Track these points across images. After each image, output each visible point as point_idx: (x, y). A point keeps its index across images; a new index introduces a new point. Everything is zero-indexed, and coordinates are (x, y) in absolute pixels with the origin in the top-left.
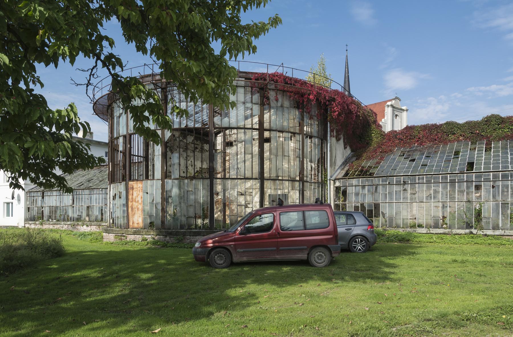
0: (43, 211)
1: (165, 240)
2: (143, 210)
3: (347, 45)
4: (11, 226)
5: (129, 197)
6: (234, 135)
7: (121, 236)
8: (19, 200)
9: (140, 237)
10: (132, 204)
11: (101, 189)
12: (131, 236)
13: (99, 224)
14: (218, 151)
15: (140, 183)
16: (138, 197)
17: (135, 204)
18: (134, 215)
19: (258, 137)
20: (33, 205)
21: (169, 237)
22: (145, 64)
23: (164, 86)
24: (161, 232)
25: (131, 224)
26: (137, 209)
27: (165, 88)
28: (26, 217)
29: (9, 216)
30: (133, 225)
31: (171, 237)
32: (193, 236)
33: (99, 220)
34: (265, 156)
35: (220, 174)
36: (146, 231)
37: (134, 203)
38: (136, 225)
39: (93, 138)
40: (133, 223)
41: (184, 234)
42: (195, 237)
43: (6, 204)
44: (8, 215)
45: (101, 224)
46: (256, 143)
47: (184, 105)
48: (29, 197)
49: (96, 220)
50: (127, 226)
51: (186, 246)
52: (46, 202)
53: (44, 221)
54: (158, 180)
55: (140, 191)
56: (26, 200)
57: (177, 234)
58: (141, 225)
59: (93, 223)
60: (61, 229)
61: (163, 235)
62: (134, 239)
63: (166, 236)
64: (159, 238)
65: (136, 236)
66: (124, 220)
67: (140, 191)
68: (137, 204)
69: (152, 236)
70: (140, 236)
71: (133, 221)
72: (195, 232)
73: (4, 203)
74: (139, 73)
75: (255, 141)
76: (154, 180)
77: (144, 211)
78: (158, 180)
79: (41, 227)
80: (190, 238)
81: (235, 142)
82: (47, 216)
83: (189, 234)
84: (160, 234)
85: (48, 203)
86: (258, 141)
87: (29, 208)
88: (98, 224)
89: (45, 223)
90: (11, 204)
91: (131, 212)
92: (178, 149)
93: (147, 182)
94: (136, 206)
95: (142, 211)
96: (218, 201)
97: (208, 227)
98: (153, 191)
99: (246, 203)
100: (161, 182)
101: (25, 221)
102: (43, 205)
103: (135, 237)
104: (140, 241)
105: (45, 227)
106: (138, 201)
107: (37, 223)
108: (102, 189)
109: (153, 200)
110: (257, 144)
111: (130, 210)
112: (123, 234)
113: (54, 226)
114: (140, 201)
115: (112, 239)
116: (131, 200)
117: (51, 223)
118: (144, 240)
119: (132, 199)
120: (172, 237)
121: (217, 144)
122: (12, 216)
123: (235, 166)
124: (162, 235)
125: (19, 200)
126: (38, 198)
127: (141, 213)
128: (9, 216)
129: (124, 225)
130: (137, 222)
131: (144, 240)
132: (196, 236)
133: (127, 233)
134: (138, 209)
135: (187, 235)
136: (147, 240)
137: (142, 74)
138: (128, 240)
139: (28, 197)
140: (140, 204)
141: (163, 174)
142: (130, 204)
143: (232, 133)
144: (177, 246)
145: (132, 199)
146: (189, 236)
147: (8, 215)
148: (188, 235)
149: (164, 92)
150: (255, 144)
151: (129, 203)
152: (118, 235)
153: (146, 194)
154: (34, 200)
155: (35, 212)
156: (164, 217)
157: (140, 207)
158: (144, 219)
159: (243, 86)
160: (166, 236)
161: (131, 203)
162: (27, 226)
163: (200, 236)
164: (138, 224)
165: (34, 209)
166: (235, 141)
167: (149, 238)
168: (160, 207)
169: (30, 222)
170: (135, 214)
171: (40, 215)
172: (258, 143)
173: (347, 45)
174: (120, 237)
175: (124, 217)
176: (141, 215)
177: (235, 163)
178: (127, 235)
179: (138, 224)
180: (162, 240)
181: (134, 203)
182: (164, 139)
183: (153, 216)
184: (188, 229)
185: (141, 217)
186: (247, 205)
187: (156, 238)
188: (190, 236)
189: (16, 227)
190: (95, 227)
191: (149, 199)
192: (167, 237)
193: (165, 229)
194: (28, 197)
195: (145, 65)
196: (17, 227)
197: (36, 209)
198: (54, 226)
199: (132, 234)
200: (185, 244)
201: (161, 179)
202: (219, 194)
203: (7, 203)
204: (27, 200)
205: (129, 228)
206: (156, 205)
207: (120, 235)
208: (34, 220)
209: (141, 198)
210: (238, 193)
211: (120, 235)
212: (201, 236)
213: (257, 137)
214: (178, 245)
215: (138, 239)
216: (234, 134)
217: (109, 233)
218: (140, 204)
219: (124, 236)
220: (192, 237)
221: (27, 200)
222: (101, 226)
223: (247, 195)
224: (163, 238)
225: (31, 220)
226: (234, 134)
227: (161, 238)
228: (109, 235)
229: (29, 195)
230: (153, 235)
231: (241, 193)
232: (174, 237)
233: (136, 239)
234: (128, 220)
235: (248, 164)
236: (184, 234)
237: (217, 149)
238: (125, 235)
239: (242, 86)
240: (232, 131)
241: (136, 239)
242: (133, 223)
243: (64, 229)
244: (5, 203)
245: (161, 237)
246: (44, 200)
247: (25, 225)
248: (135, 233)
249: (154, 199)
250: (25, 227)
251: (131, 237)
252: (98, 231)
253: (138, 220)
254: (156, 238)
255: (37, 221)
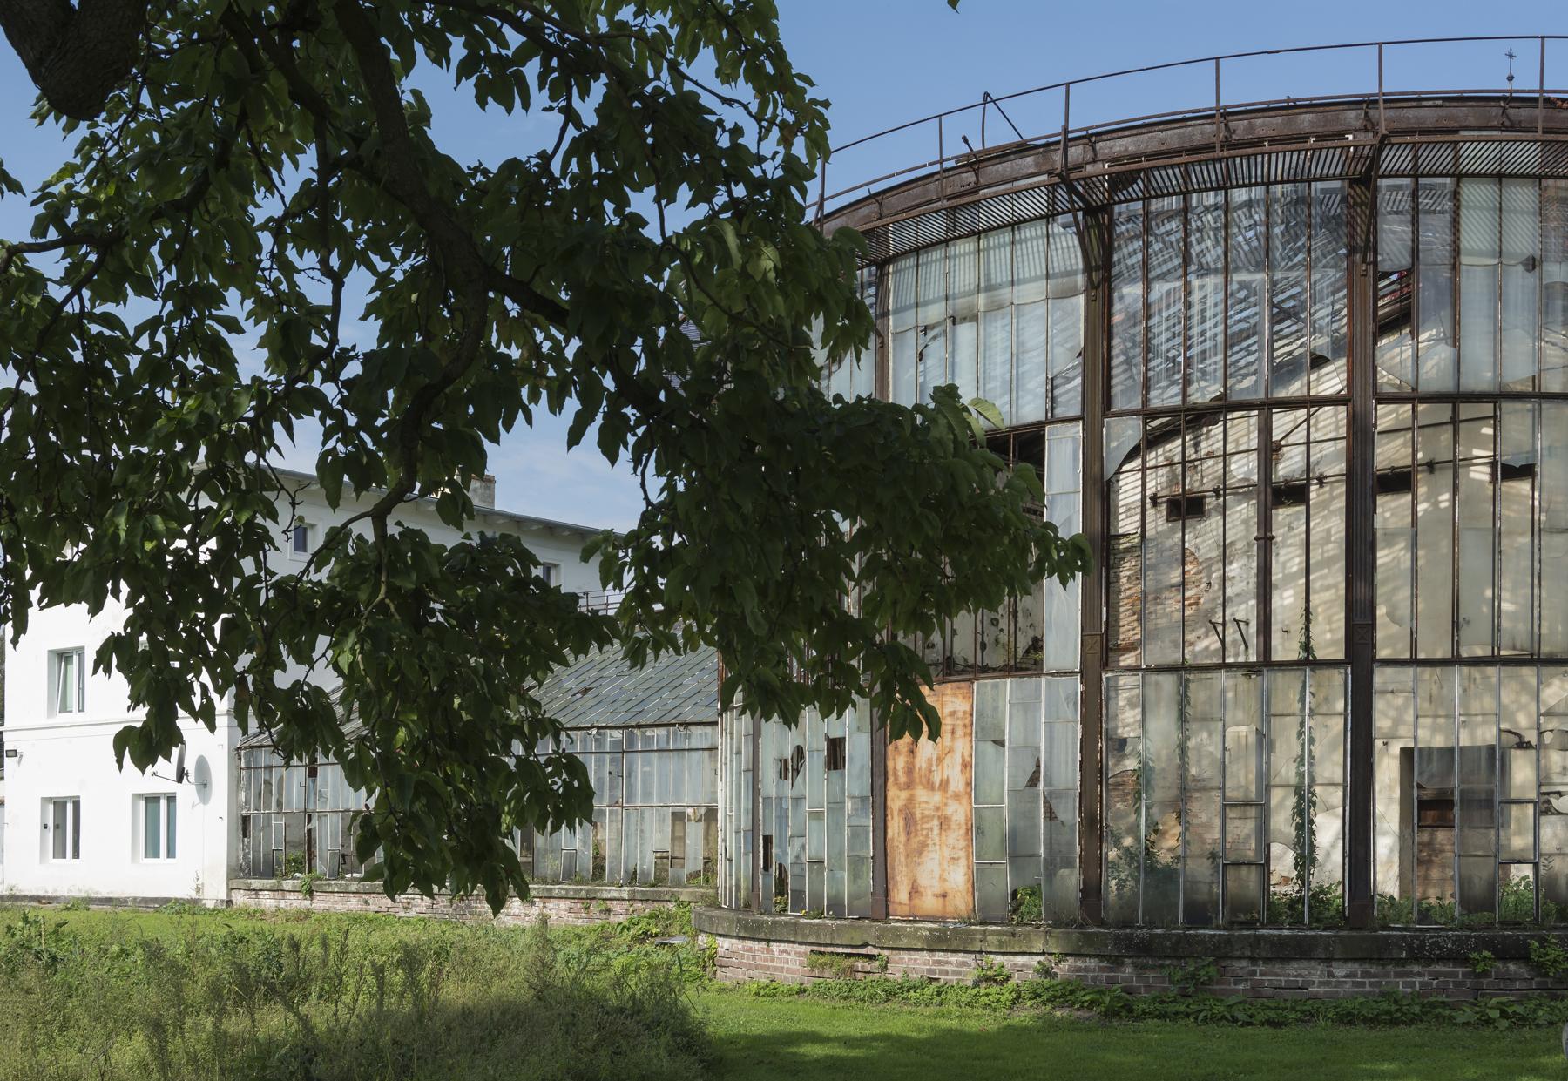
0: (309, 831)
1: (1114, 982)
2: (977, 830)
3: (1511, 56)
4: (177, 900)
5: (890, 765)
6: (1210, 462)
7: (849, 955)
8: (204, 784)
9: (964, 964)
10: (911, 799)
11: (594, 732)
12: (915, 955)
13: (588, 892)
14: (1125, 544)
15: (955, 695)
16: (947, 760)
17: (926, 799)
18: (920, 853)
19: (1344, 465)
20: (268, 806)
21: (1135, 966)
22: (987, 95)
23: (1098, 197)
24: (1088, 939)
25: (900, 894)
26: (936, 822)
27: (1106, 208)
28: (234, 863)
29: (64, 857)
30: (916, 901)
31: (1144, 967)
32: (1267, 960)
33: (584, 873)
34: (1379, 562)
35: (1133, 654)
36: (1000, 934)
37: (921, 794)
38: (929, 904)
39: (493, 502)
40: (914, 891)
41: (1221, 952)
42: (1277, 968)
43: (142, 803)
44: (152, 850)
45: (596, 891)
46: (1333, 498)
47: (1210, 288)
48: (248, 768)
49: (570, 875)
50: (881, 905)
51: (1241, 1016)
52: (329, 792)
53: (319, 879)
54: (1066, 673)
55: (959, 732)
56: (235, 783)
57: (1180, 950)
58: (961, 902)
59: (556, 889)
60: (402, 914)
61: (1101, 957)
62: (929, 971)
63: (1116, 961)
64: (1079, 969)
65: (940, 956)
66: (855, 876)
67: (959, 732)
68: (937, 797)
69: (1041, 958)
70: (969, 958)
71: (915, 881)
72: (1281, 943)
73: (137, 796)
74: (965, 140)
75: (1327, 488)
76: (1040, 674)
77: (980, 831)
78: (1066, 673)
79: (308, 903)
80: (1253, 973)
81: (1218, 496)
82: (334, 854)
83: (1248, 953)
84: (1084, 950)
85: (336, 798)
86: (1344, 489)
87: (245, 820)
88: (583, 894)
89: (326, 888)
90: (163, 803)
91: (903, 838)
92: (1127, 524)
93: (995, 686)
94: (931, 806)
95: (968, 830)
96: (1123, 784)
97: (1340, 913)
98: (1036, 730)
99: (1544, 789)
100: (1080, 688)
101: (229, 879)
102: (311, 808)
103: (939, 962)
104: (970, 983)
105: (321, 903)
106: (945, 785)
107: (288, 884)
108: (599, 728)
109: (1033, 781)
110: (1340, 503)
111: (895, 827)
112: (865, 945)
113: (366, 902)
114: (958, 783)
115: (793, 972)
116: (903, 779)
117: (354, 887)
118: (988, 979)
119: (910, 770)
120: (1153, 968)
121: (1121, 510)
122: (76, 855)
123: (1213, 611)
124: (1097, 956)
125: (205, 785)
126: (290, 777)
127: (962, 843)
128: (64, 857)
129: (856, 903)
130: (938, 890)
131: (988, 979)
132: (1286, 960)
133: (891, 944)
134: (945, 823)
135: (1232, 958)
136: (1008, 978)
137: (977, 147)
138: (895, 974)
139: (244, 772)
140: (957, 796)
141: (1089, 641)
142: (896, 798)
143: (1203, 453)
144: (1188, 1015)
145: (910, 770)
146: (1244, 963)
147: (152, 850)
148: (1239, 958)
149: (1099, 226)
150: (1324, 505)
151: (892, 792)
152: (830, 949)
153: (990, 748)
154: (268, 783)
155: (275, 835)
156: (1093, 863)
157: (959, 812)
158: (978, 878)
159: (1491, 175)
160: (1116, 961)
161: (904, 795)
162: (240, 898)
163: (1304, 964)
164: (944, 896)
165: (270, 825)
166: (1216, 492)
167: (1024, 967)
168: (1071, 814)
169: (256, 883)
170: (924, 845)
171: (299, 853)
172: (1344, 498)
173: (1511, 56)
174: (847, 963)
175: (857, 862)
176: (962, 854)
177: (1214, 599)
178: (886, 952)
179: (944, 896)
180: (1094, 979)
181: (921, 794)
182: (1098, 464)
183: (1036, 855)
184: (1231, 925)
185: (963, 862)
186: (1548, 802)
187: (1064, 968)
188: (1253, 959)
189: (191, 907)
190: (563, 905)
191: (1006, 772)
192: (1122, 964)
193: (1103, 924)
194: (244, 772)
195: (985, 102)
196: (195, 902)
197: (278, 823)
198: (366, 902)
199: (922, 950)
200: (1231, 1001)
201: (1081, 672)
202: (1128, 750)
203: (55, 803)
204: (239, 782)
205: (887, 914)
206: (1054, 803)
207: (840, 950)
208: (272, 875)
209: (965, 766)
210: (1504, 736)
211: (840, 950)
212: (1313, 963)
213: (1341, 467)
214: (1194, 1007)
215: (955, 973)
216: (1210, 456)
217: (768, 941)
218: (957, 796)
219: (872, 957)
220: (1261, 967)
221: (239, 782)
222: (594, 902)
223: (1547, 747)
224: (1101, 969)
225: (257, 873)
226: (1210, 456)
227: (1086, 969)
228: (769, 951)
229: (248, 762)
230: (1043, 954)
231: (1517, 739)
232: (1162, 966)
233: (946, 973)
234: (880, 879)
235: (1291, 600)
236: (1221, 952)
237: (1121, 531)
238: (875, 951)
239: (1485, 175)
240: (1203, 445)
241: (946, 973)
242: (914, 891)
243: (413, 913)
244: (140, 796)
245: (1092, 963)
246: (314, 782)
247: (229, 895)
248: (936, 943)
249: (1037, 772)
250: (230, 902)
251: (910, 965)
252: (579, 923)
253: (943, 880)
254: (1064, 968)
255: (285, 876)
